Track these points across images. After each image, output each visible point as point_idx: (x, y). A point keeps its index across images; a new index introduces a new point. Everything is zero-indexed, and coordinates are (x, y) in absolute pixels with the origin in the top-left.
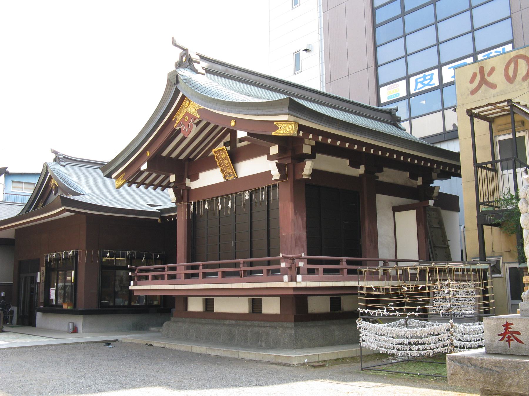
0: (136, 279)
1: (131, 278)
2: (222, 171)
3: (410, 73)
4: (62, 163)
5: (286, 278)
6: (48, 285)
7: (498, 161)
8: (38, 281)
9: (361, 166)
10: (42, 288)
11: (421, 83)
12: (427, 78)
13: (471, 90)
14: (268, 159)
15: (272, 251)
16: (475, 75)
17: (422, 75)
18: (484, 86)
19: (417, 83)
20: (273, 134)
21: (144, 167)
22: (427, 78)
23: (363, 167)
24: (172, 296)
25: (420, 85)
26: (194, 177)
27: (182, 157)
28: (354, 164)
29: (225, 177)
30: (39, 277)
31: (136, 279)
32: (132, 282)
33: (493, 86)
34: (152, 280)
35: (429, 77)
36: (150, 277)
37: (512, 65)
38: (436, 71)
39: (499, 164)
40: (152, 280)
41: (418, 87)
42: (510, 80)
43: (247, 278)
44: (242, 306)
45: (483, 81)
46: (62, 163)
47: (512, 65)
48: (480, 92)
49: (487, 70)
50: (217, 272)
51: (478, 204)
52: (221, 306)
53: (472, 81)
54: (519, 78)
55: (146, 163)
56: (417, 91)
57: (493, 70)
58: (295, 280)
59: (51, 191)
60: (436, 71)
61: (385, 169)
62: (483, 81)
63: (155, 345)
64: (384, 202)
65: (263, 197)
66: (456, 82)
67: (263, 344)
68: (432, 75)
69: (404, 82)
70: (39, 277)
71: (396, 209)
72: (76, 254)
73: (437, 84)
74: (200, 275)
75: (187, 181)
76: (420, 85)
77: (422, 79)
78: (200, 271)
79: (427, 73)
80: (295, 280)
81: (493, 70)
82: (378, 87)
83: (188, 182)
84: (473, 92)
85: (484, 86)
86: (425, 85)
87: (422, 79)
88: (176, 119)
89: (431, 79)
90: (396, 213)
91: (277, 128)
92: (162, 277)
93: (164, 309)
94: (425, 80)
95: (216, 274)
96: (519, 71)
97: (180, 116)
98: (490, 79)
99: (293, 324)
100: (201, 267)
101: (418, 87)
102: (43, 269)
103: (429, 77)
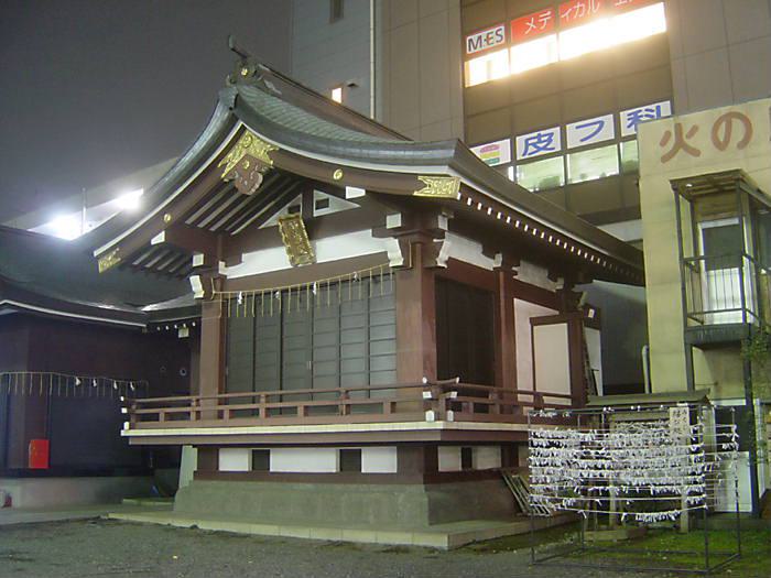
0: (133, 420)
1: (127, 417)
2: (289, 251)
5: (430, 415)
7: (702, 258)
9: (497, 256)
11: (534, 144)
12: (543, 139)
13: (660, 156)
14: (373, 236)
15: (284, 386)
16: (668, 134)
18: (681, 150)
19: (527, 145)
20: (416, 194)
22: (543, 139)
23: (499, 257)
25: (531, 149)
26: (234, 260)
28: (489, 252)
29: (292, 261)
31: (133, 420)
32: (127, 425)
33: (696, 153)
34: (166, 420)
35: (546, 138)
36: (162, 416)
37: (724, 125)
39: (703, 262)
40: (166, 420)
41: (529, 151)
42: (721, 146)
43: (284, 419)
44: (327, 462)
45: (680, 144)
47: (724, 125)
48: (675, 159)
49: (686, 131)
50: (158, 414)
51: (687, 316)
52: (279, 462)
53: (663, 143)
54: (733, 143)
55: (163, 233)
56: (527, 156)
57: (694, 129)
58: (445, 419)
61: (522, 262)
62: (680, 144)
63: (200, 526)
64: (523, 309)
65: (148, 308)
66: (639, 137)
67: (371, 518)
71: (535, 322)
73: (558, 149)
74: (262, 413)
76: (531, 149)
77: (536, 140)
78: (262, 406)
80: (445, 419)
81: (694, 129)
83: (223, 269)
84: (665, 159)
85: (681, 150)
86: (539, 149)
87: (536, 140)
88: (225, 166)
89: (550, 141)
90: (535, 328)
91: (422, 185)
92: (255, 413)
94: (540, 142)
95: (293, 410)
96: (733, 135)
97: (233, 159)
98: (690, 142)
99: (423, 486)
100: (263, 400)
101: (529, 151)
103: (546, 138)
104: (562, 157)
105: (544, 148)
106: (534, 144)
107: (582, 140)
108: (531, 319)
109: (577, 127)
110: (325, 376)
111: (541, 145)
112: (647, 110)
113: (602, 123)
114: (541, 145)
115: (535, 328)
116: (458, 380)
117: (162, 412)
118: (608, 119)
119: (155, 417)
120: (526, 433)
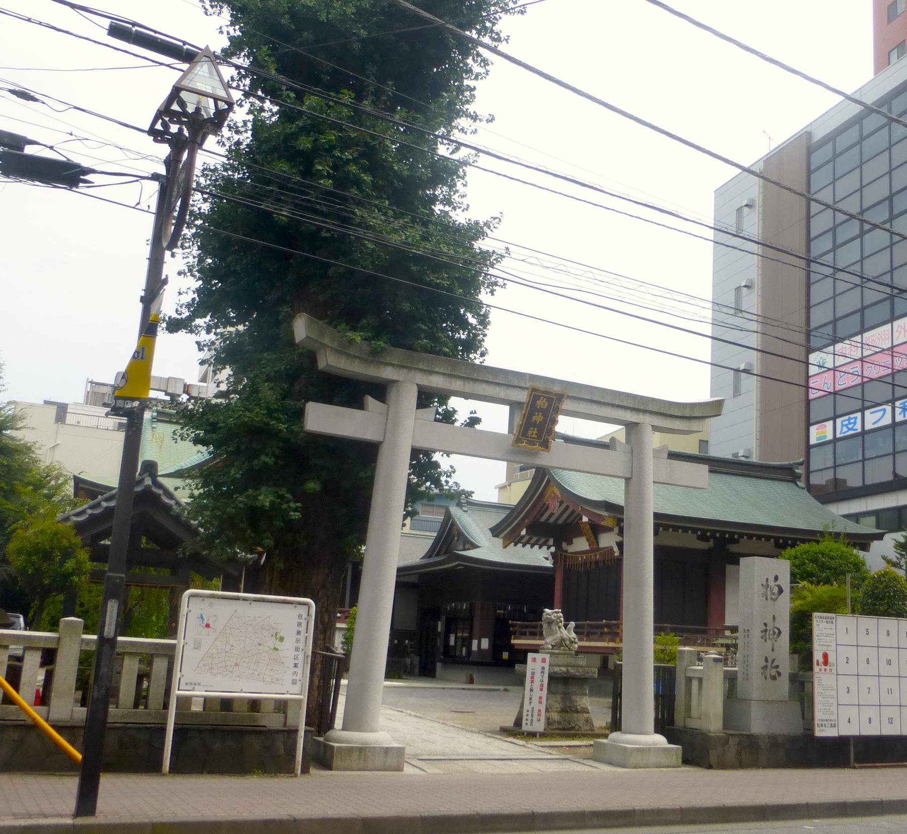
2: (588, 540)
3: (838, 413)
4: (465, 509)
6: (448, 632)
8: (439, 630)
10: (442, 636)
11: (846, 426)
17: (847, 417)
19: (843, 425)
21: (523, 532)
24: (657, 696)
27: (560, 521)
30: (440, 627)
38: (859, 415)
46: (465, 509)
59: (453, 538)
60: (859, 415)
68: (856, 418)
69: (831, 422)
70: (440, 627)
72: (472, 608)
75: (564, 545)
76: (845, 429)
79: (852, 416)
82: (808, 424)
86: (849, 429)
89: (855, 423)
93: (703, 538)
94: (850, 423)
102: (444, 618)
103: (852, 421)
104: (866, 428)
105: (852, 429)
106: (846, 426)
107: (874, 423)
108: (491, 529)
109: (872, 413)
110: (711, 228)
111: (850, 426)
112: (540, 711)
113: (884, 410)
114: (850, 426)
115: (55, 407)
116: (387, 202)
117: (528, 630)
118: (888, 408)
119: (525, 634)
120: (439, 30)
